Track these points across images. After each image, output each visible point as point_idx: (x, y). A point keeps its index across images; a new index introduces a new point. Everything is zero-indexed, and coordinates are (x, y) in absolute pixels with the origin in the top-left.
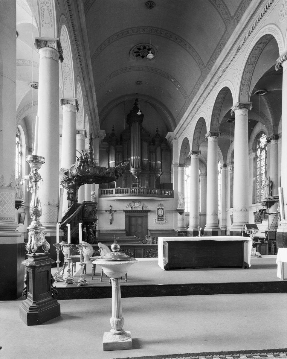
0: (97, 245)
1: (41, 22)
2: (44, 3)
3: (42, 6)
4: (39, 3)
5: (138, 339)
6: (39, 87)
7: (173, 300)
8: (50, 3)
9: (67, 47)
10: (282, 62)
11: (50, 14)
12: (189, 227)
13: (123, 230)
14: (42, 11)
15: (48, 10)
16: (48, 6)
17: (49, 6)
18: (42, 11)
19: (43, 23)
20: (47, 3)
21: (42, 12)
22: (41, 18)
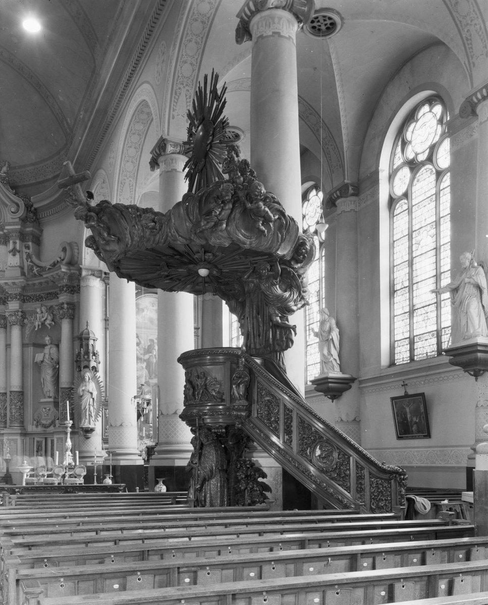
0: (153, 470)
1: (172, 111)
2: (183, 84)
3: (177, 88)
4: (175, 84)
5: (315, 4)
6: (193, 327)
7: (18, 172)
8: (191, 86)
9: (193, 80)
10: (479, 101)
12: (433, 292)
13: (194, 298)
14: (176, 94)
15: (186, 96)
16: (188, 91)
17: (190, 90)
18: (176, 94)
19: (175, 113)
20: (187, 85)
21: (177, 97)
22: (172, 105)
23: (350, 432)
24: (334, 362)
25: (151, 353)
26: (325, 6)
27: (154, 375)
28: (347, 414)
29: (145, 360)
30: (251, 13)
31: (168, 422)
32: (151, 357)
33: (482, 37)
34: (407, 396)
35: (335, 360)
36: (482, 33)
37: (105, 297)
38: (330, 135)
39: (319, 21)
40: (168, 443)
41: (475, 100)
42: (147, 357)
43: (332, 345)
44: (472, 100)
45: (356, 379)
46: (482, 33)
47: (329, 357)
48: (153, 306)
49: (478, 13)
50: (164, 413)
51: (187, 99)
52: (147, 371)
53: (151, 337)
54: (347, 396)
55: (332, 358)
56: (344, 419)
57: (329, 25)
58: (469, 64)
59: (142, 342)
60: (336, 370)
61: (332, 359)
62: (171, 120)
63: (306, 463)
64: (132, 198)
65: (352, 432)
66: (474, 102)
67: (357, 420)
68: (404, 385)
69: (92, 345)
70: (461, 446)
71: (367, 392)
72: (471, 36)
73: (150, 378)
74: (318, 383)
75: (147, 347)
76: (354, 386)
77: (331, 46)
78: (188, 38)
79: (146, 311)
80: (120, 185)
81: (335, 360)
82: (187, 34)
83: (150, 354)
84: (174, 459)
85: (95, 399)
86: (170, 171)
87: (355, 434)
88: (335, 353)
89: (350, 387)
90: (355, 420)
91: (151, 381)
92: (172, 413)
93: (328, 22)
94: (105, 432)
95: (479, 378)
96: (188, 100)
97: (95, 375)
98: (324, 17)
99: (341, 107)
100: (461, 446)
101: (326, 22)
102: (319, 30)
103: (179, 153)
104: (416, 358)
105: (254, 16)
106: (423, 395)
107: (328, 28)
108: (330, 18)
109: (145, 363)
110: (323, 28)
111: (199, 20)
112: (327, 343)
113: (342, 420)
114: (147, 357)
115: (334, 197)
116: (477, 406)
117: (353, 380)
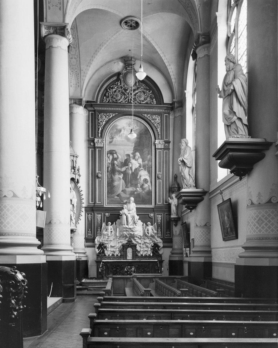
11: (77, 77)
20: (75, 69)
23: (263, 219)
24: (239, 123)
25: (127, 165)
27: (129, 184)
28: (259, 193)
29: (122, 172)
32: (128, 170)
35: (240, 119)
37: (88, 122)
42: (123, 169)
43: (235, 99)
47: (231, 116)
48: (129, 126)
52: (123, 181)
53: (127, 153)
55: (235, 118)
56: (255, 201)
59: (120, 157)
60: (240, 132)
64: (60, 4)
65: (266, 219)
67: (272, 201)
69: (75, 161)
70: (218, 248)
73: (127, 187)
75: (123, 161)
79: (123, 130)
81: (240, 119)
83: (127, 167)
84: (61, 256)
85: (75, 205)
87: (272, 224)
88: (240, 111)
91: (128, 190)
94: (88, 233)
97: (77, 185)
100: (218, 248)
109: (122, 175)
112: (230, 98)
113: (252, 203)
114: (123, 169)
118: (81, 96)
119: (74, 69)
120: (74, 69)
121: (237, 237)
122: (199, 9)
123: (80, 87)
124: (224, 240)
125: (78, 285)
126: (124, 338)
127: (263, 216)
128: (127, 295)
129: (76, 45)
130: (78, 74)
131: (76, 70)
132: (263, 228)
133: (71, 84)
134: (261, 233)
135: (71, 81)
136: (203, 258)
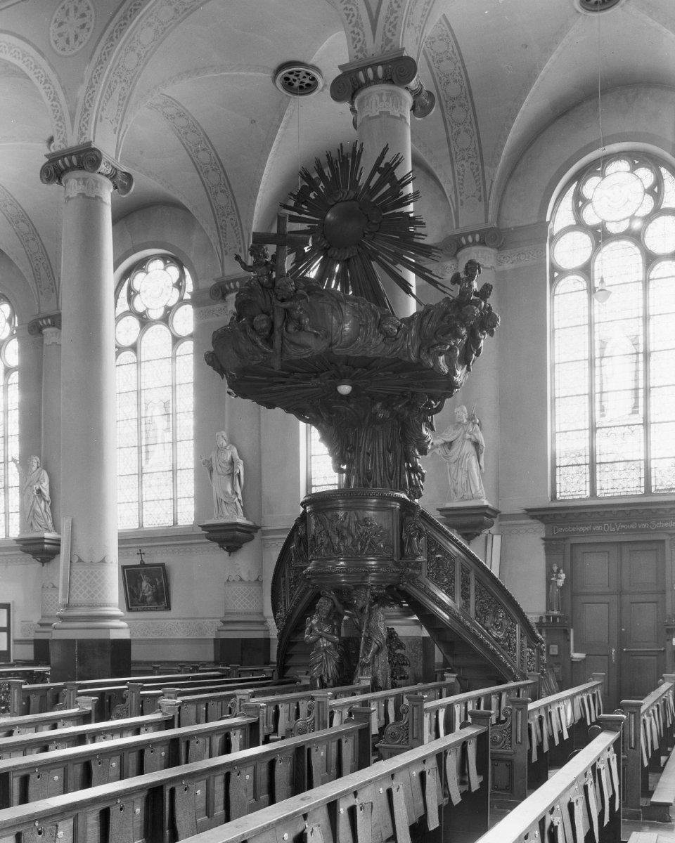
10: (468, 244)
24: (238, 503)
26: (317, 65)
30: (374, 78)
31: (92, 573)
33: (476, 179)
34: (143, 564)
36: (478, 175)
38: (234, 205)
39: (297, 76)
40: (92, 606)
41: (464, 241)
44: (460, 239)
45: (260, 528)
46: (478, 175)
47: (233, 497)
49: (478, 153)
50: (85, 559)
51: (120, 99)
54: (247, 551)
56: (245, 577)
57: (304, 85)
58: (456, 201)
61: (236, 499)
62: (98, 123)
63: (426, 599)
64: (240, 243)
65: (255, 595)
66: (461, 243)
68: (141, 553)
71: (273, 545)
72: (464, 172)
74: (212, 529)
76: (257, 536)
77: (290, 107)
78: (150, 20)
80: (221, 231)
82: (152, 15)
84: (109, 628)
86: (93, 198)
89: (252, 538)
90: (258, 580)
92: (100, 560)
93: (307, 81)
95: (45, 564)
96: (121, 102)
98: (308, 74)
99: (264, 178)
101: (303, 80)
102: (291, 84)
103: (107, 176)
104: (558, 495)
105: (376, 84)
106: (163, 565)
107: (301, 87)
108: (313, 79)
110: (297, 84)
111: (457, 105)
115: (230, 287)
116: (228, 580)
117: (255, 529)
118: (486, 222)
119: (466, 158)
120: (466, 158)
121: (168, 608)
122: (450, 197)
123: (483, 200)
124: (168, 608)
125: (479, 707)
126: (68, 638)
127: (253, 592)
128: (463, 730)
129: (465, 97)
130: (477, 169)
131: (470, 160)
132: (253, 603)
133: (461, 198)
134: (240, 608)
135: (462, 191)
136: (262, 632)
